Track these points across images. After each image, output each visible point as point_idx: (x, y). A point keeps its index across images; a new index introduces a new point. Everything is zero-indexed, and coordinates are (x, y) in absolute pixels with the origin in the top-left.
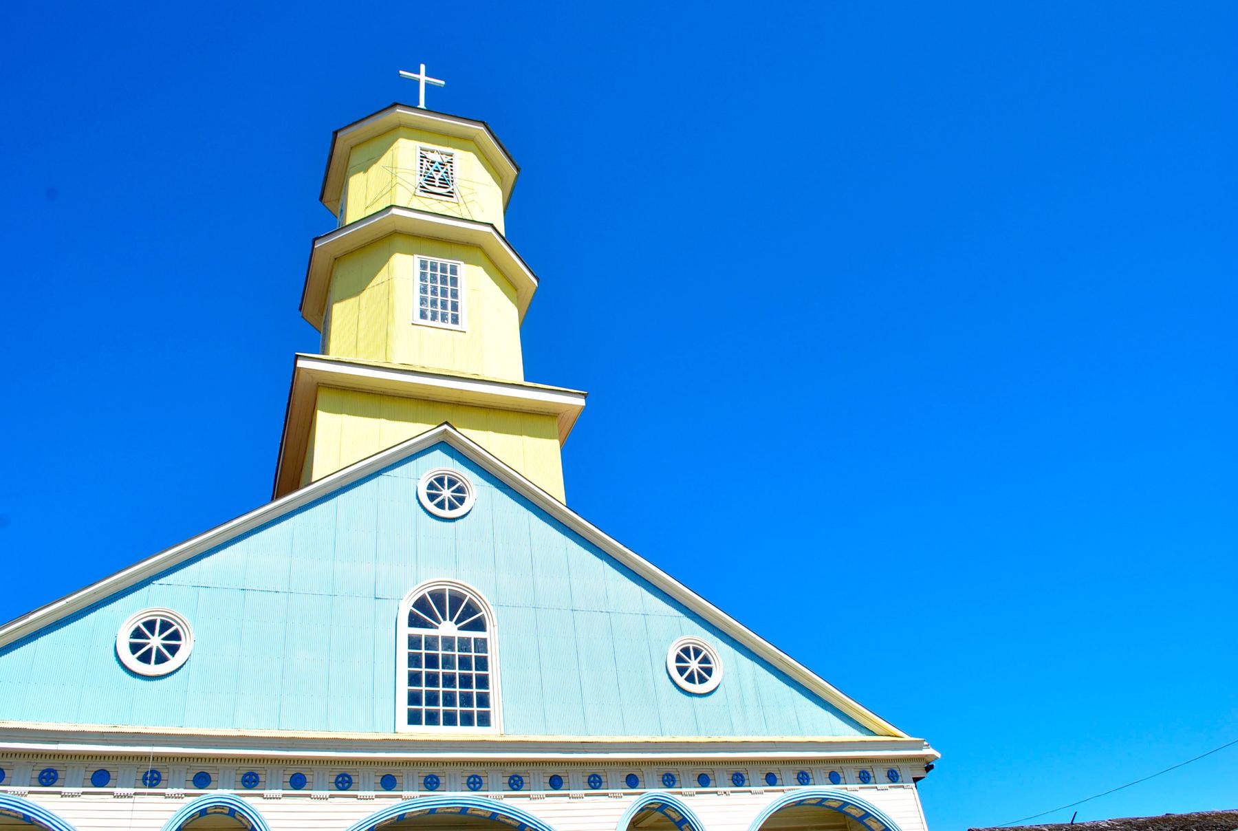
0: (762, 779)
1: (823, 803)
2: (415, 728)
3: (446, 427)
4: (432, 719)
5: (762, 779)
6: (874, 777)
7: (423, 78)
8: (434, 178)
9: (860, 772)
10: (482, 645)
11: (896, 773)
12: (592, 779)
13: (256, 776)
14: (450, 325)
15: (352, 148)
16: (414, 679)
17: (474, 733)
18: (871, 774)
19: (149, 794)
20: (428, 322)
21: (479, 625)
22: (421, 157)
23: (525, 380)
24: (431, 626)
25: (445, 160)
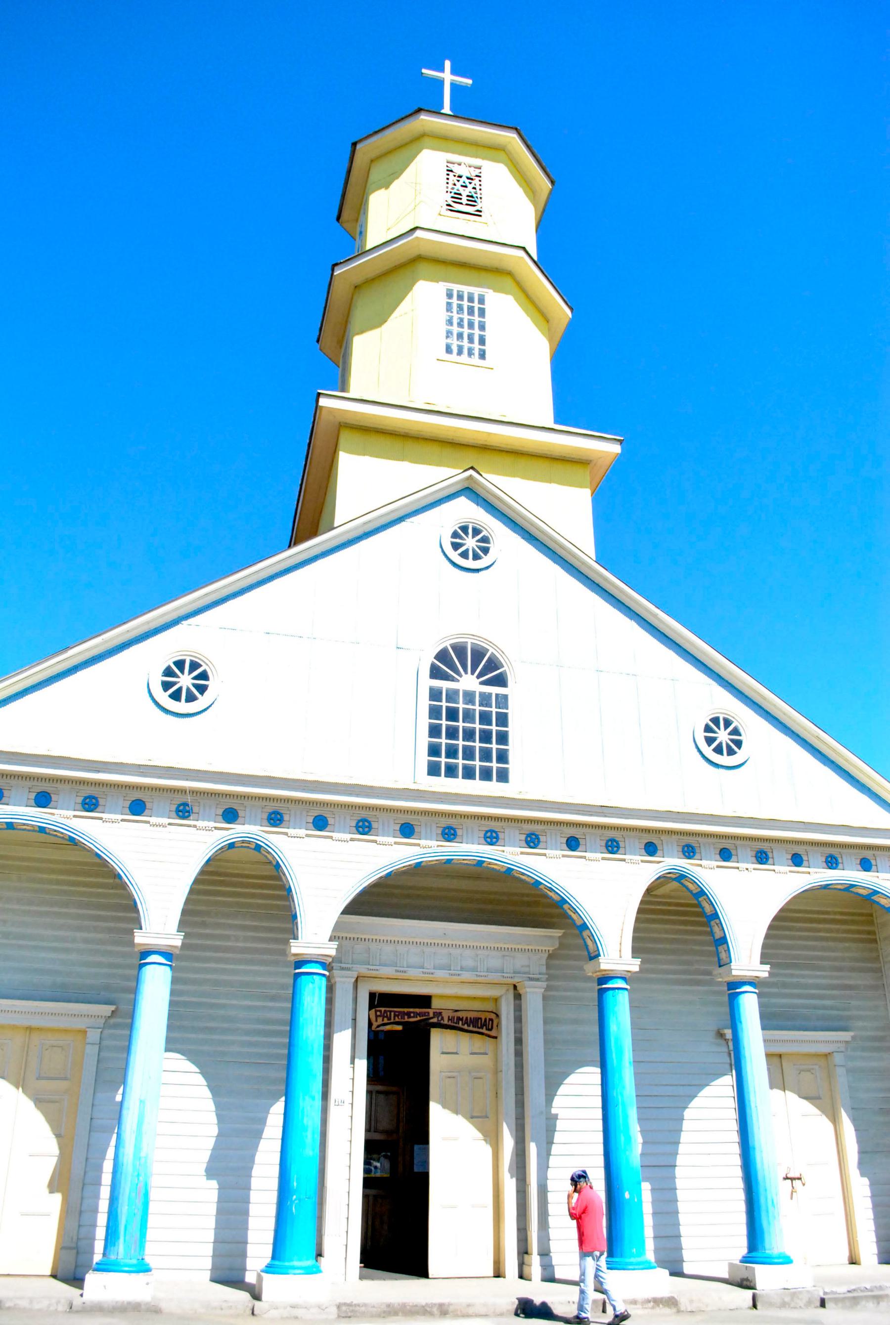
2: (442, 784)
3: (471, 472)
4: (451, 771)
6: (773, 858)
10: (503, 701)
16: (434, 731)
17: (492, 788)
24: (453, 679)
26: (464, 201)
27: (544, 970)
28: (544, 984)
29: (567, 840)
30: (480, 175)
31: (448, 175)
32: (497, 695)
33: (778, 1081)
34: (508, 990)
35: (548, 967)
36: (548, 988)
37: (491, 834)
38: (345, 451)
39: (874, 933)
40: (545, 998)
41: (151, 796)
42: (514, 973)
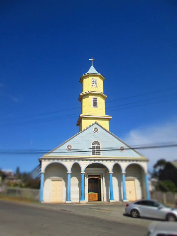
2: (93, 155)
4: (95, 155)
7: (92, 60)
10: (100, 147)
14: (96, 107)
19: (103, 192)
20: (94, 107)
21: (99, 145)
23: (106, 114)
24: (94, 145)
33: (82, 130)
38: (83, 119)
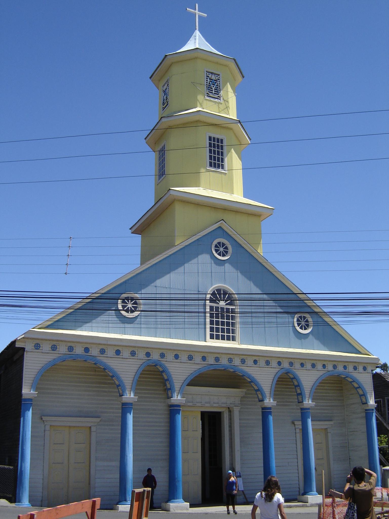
0: (129, 354)
1: (346, 378)
4: (218, 338)
5: (129, 354)
8: (212, 88)
9: (312, 364)
11: (366, 368)
12: (132, 352)
13: (164, 354)
15: (172, 63)
18: (358, 367)
22: (207, 76)
25: (217, 78)
26: (214, 90)
27: (240, 402)
28: (240, 408)
29: (254, 361)
30: (219, 79)
31: (207, 78)
32: (231, 308)
34: (226, 409)
35: (241, 401)
36: (241, 408)
37: (230, 359)
39: (342, 387)
40: (240, 412)
41: (122, 348)
42: (230, 404)
